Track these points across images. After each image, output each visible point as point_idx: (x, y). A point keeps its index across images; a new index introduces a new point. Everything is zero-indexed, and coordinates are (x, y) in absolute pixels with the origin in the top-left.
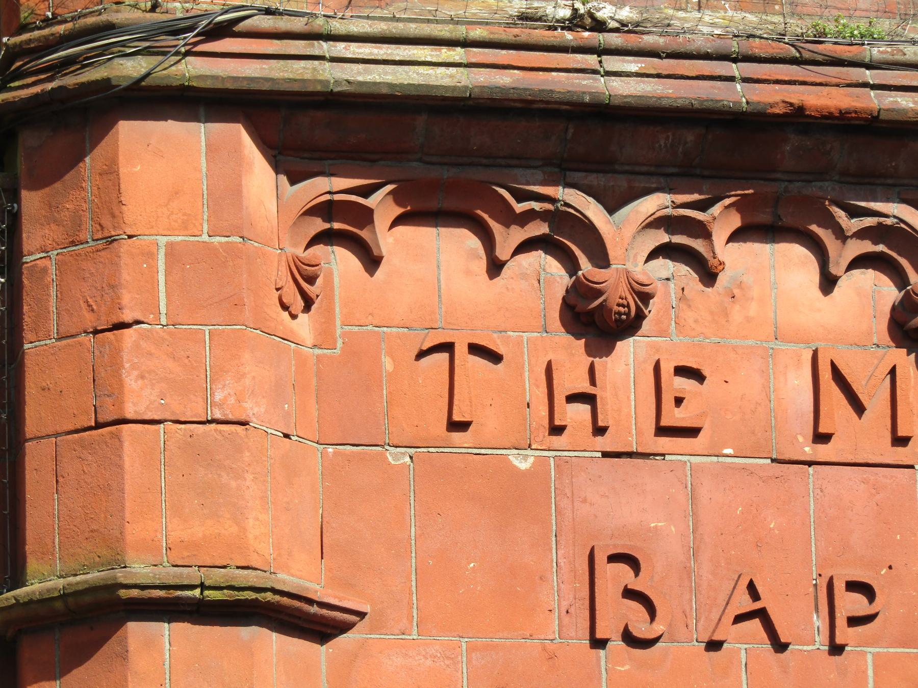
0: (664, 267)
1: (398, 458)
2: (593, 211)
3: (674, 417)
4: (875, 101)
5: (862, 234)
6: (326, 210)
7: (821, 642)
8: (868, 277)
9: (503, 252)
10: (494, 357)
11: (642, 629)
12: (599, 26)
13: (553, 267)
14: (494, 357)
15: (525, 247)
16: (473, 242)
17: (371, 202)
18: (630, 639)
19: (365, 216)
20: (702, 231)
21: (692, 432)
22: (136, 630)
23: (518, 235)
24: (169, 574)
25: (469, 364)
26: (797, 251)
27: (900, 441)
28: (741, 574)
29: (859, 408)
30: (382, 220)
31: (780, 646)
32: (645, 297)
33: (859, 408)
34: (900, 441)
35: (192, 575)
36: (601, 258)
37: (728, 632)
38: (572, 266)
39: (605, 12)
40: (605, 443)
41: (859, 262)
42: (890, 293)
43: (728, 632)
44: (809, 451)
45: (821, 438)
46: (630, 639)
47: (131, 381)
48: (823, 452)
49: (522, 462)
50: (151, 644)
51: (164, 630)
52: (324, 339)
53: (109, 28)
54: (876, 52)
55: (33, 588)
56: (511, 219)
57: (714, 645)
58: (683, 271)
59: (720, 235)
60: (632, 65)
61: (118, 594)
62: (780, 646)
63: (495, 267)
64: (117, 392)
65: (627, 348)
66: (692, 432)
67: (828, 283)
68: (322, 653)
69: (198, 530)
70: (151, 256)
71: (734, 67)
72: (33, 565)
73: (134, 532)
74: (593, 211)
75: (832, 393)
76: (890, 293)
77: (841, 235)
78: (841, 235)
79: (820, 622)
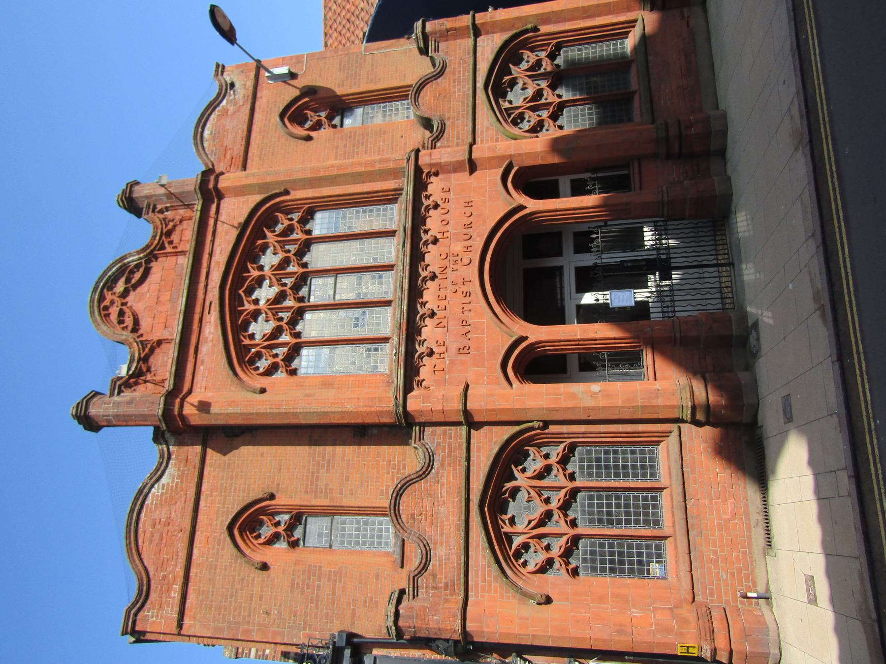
0: (424, 345)
1: (447, 377)
2: (418, 354)
3: (442, 344)
4: (405, 320)
5: (421, 321)
6: (418, 385)
7: (469, 327)
8: (426, 321)
9: (422, 364)
10: (435, 365)
11: (468, 348)
12: (396, 353)
13: (424, 358)
14: (435, 365)
15: (422, 361)
16: (421, 368)
17: (417, 380)
18: (469, 349)
19: (419, 381)
20: (420, 341)
21: (446, 296)
22: (468, 408)
23: (421, 362)
24: (461, 404)
25: (436, 369)
26: (423, 329)
27: (445, 317)
28: (693, 603)
29: (441, 322)
30: (419, 379)
31: (469, 332)
32: (428, 347)
33: (441, 322)
34: (445, 317)
35: (461, 401)
36: (423, 353)
37: (468, 337)
38: (424, 356)
39: (394, 352)
40: (445, 352)
41: (424, 322)
42: (428, 319)
43: (468, 337)
44: (446, 328)
45: (445, 327)
46: (469, 349)
47: (438, 409)
48: (446, 326)
49: (448, 362)
50: (470, 406)
51: (468, 404)
52: (433, 385)
53: (396, 411)
54: (399, 320)
55: (463, 420)
56: (419, 363)
57: (469, 339)
58: (425, 343)
59: (421, 339)
60: (401, 349)
61: (511, 656)
62: (469, 332)
63: (424, 365)
64: (439, 410)
65: (434, 350)
66: (446, 296)
67: (426, 326)
68: (470, 386)
69: (456, 400)
70: (423, 406)
71: (324, 369)
72: (460, 420)
73: (456, 408)
74: (418, 354)
75: (439, 325)
76: (428, 319)
77: (421, 324)
78: (421, 324)
79: (466, 327)
